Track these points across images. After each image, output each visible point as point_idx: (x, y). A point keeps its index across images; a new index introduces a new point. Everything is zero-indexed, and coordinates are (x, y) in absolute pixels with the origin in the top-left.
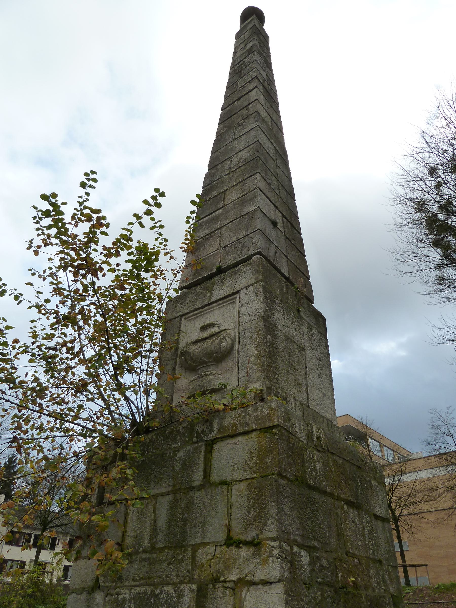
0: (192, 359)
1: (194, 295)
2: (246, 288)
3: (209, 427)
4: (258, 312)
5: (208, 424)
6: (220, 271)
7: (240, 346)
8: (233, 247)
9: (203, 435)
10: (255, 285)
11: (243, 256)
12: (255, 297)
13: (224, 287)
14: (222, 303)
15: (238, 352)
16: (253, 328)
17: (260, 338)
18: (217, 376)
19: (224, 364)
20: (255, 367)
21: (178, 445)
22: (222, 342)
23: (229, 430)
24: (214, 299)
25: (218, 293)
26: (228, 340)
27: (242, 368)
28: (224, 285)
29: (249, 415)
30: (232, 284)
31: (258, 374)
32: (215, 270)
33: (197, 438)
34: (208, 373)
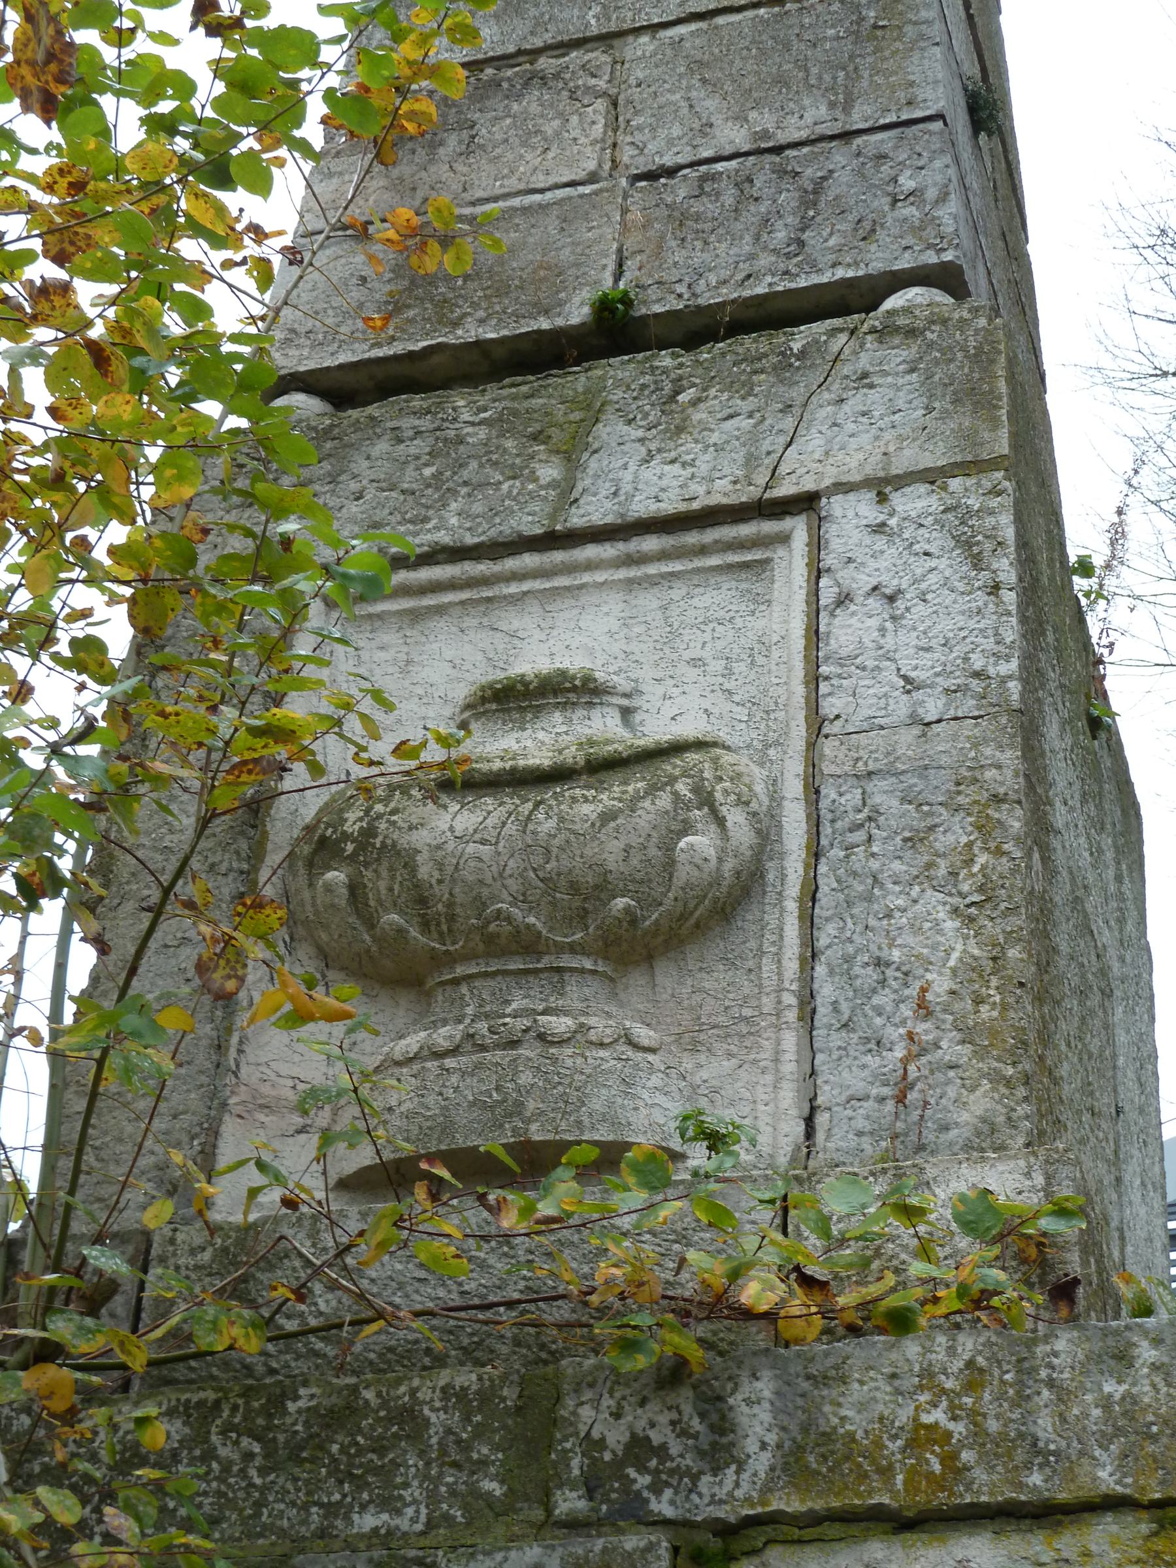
0: (420, 900)
1: (419, 447)
2: (882, 487)
3: (696, 1424)
4: (977, 675)
5: (685, 1399)
6: (616, 331)
7: (826, 884)
8: (729, 197)
9: (644, 1480)
10: (955, 484)
11: (815, 268)
12: (949, 565)
13: (688, 447)
14: (663, 556)
15: (808, 921)
16: (942, 780)
17: (999, 852)
18: (642, 1067)
19: (666, 976)
20: (951, 1049)
21: (403, 1523)
22: (687, 828)
23: (886, 1472)
24: (595, 510)
25: (633, 474)
26: (735, 817)
27: (837, 1039)
28: (680, 430)
29: (1051, 1383)
30: (753, 438)
31: (981, 1102)
32: (577, 312)
33: (590, 1495)
34: (561, 1024)
